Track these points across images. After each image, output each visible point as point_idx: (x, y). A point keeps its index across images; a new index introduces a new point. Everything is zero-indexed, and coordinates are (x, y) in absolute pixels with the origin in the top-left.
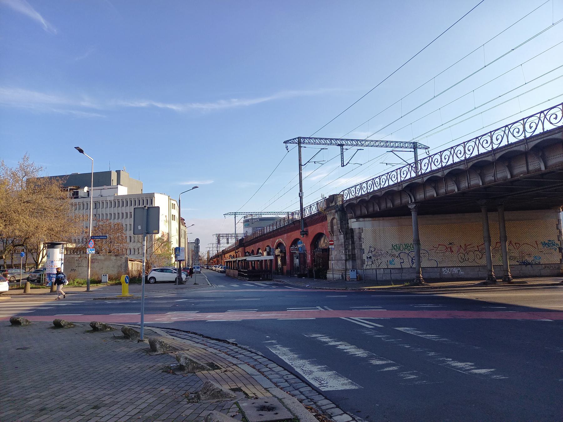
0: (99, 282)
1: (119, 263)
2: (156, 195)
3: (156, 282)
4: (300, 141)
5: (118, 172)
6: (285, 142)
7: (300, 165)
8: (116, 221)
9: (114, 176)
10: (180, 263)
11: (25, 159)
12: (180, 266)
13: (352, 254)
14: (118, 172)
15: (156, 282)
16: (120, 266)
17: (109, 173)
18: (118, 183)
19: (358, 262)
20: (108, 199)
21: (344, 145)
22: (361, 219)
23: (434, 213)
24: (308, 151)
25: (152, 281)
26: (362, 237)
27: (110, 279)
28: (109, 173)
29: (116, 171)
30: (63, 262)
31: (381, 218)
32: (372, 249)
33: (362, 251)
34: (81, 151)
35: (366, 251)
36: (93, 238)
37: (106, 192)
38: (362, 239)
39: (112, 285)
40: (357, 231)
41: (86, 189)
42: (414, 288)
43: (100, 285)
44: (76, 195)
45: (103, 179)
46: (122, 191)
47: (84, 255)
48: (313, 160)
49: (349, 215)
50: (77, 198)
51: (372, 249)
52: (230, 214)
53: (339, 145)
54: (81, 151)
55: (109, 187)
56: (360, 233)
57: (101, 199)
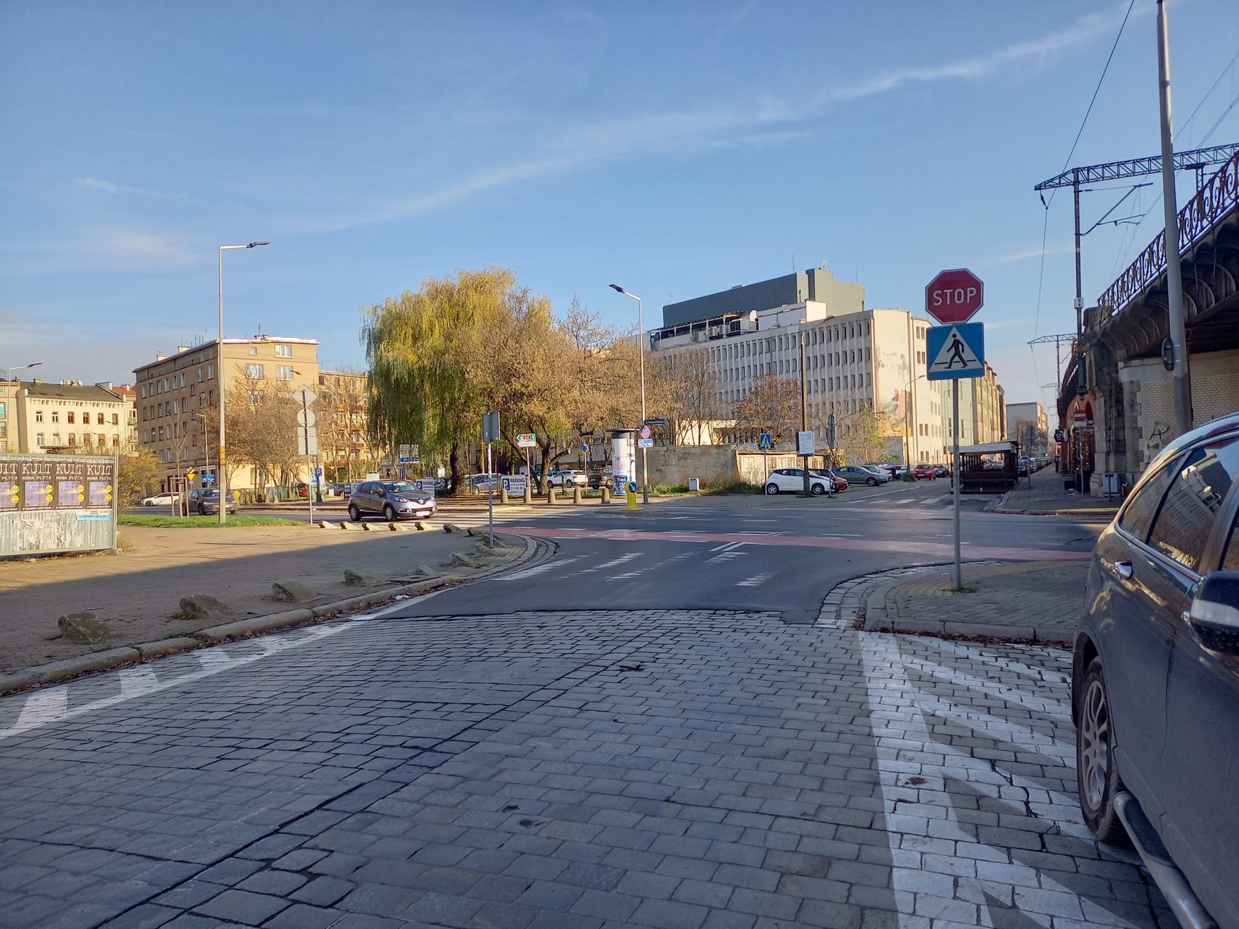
0: (686, 490)
1: (723, 459)
2: (876, 314)
3: (779, 492)
4: (1077, 179)
5: (811, 274)
6: (1038, 188)
7: (1078, 234)
8: (784, 377)
9: (802, 284)
10: (806, 460)
11: (575, 302)
12: (806, 466)
13: (1118, 440)
14: (811, 274)
15: (779, 492)
16: (725, 465)
17: (793, 278)
18: (812, 296)
19: (1129, 456)
20: (790, 331)
21: (1204, 164)
22: (1135, 362)
23: (1215, 349)
24: (1097, 198)
25: (773, 489)
26: (1138, 401)
27: (702, 486)
28: (793, 278)
29: (807, 272)
30: (633, 458)
31: (1232, 351)
32: (1162, 428)
33: (1138, 432)
34: (619, 290)
35: (1146, 433)
36: (647, 422)
37: (784, 316)
38: (1137, 407)
39: (704, 495)
40: (1126, 389)
41: (753, 315)
42: (1077, 514)
43: (686, 495)
44: (735, 330)
45: (780, 292)
46: (816, 312)
47: (671, 447)
48: (1111, 218)
49: (1120, 353)
50: (739, 334)
51: (1162, 428)
52: (1044, 340)
53: (1189, 167)
54: (619, 290)
55: (792, 306)
56: (1133, 394)
57: (777, 333)
